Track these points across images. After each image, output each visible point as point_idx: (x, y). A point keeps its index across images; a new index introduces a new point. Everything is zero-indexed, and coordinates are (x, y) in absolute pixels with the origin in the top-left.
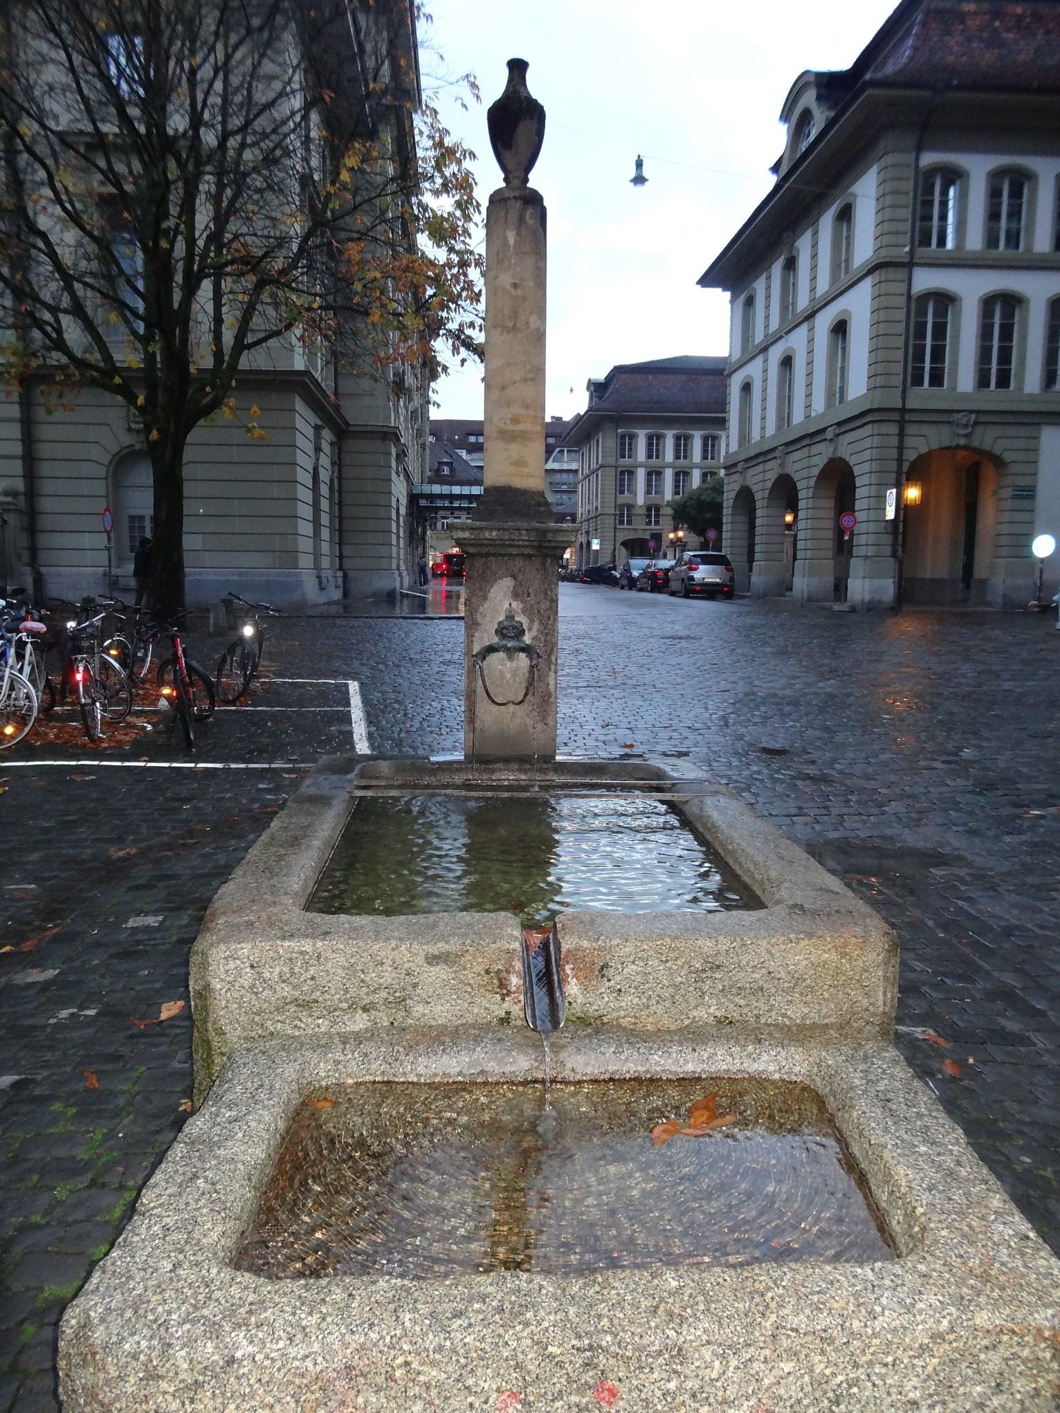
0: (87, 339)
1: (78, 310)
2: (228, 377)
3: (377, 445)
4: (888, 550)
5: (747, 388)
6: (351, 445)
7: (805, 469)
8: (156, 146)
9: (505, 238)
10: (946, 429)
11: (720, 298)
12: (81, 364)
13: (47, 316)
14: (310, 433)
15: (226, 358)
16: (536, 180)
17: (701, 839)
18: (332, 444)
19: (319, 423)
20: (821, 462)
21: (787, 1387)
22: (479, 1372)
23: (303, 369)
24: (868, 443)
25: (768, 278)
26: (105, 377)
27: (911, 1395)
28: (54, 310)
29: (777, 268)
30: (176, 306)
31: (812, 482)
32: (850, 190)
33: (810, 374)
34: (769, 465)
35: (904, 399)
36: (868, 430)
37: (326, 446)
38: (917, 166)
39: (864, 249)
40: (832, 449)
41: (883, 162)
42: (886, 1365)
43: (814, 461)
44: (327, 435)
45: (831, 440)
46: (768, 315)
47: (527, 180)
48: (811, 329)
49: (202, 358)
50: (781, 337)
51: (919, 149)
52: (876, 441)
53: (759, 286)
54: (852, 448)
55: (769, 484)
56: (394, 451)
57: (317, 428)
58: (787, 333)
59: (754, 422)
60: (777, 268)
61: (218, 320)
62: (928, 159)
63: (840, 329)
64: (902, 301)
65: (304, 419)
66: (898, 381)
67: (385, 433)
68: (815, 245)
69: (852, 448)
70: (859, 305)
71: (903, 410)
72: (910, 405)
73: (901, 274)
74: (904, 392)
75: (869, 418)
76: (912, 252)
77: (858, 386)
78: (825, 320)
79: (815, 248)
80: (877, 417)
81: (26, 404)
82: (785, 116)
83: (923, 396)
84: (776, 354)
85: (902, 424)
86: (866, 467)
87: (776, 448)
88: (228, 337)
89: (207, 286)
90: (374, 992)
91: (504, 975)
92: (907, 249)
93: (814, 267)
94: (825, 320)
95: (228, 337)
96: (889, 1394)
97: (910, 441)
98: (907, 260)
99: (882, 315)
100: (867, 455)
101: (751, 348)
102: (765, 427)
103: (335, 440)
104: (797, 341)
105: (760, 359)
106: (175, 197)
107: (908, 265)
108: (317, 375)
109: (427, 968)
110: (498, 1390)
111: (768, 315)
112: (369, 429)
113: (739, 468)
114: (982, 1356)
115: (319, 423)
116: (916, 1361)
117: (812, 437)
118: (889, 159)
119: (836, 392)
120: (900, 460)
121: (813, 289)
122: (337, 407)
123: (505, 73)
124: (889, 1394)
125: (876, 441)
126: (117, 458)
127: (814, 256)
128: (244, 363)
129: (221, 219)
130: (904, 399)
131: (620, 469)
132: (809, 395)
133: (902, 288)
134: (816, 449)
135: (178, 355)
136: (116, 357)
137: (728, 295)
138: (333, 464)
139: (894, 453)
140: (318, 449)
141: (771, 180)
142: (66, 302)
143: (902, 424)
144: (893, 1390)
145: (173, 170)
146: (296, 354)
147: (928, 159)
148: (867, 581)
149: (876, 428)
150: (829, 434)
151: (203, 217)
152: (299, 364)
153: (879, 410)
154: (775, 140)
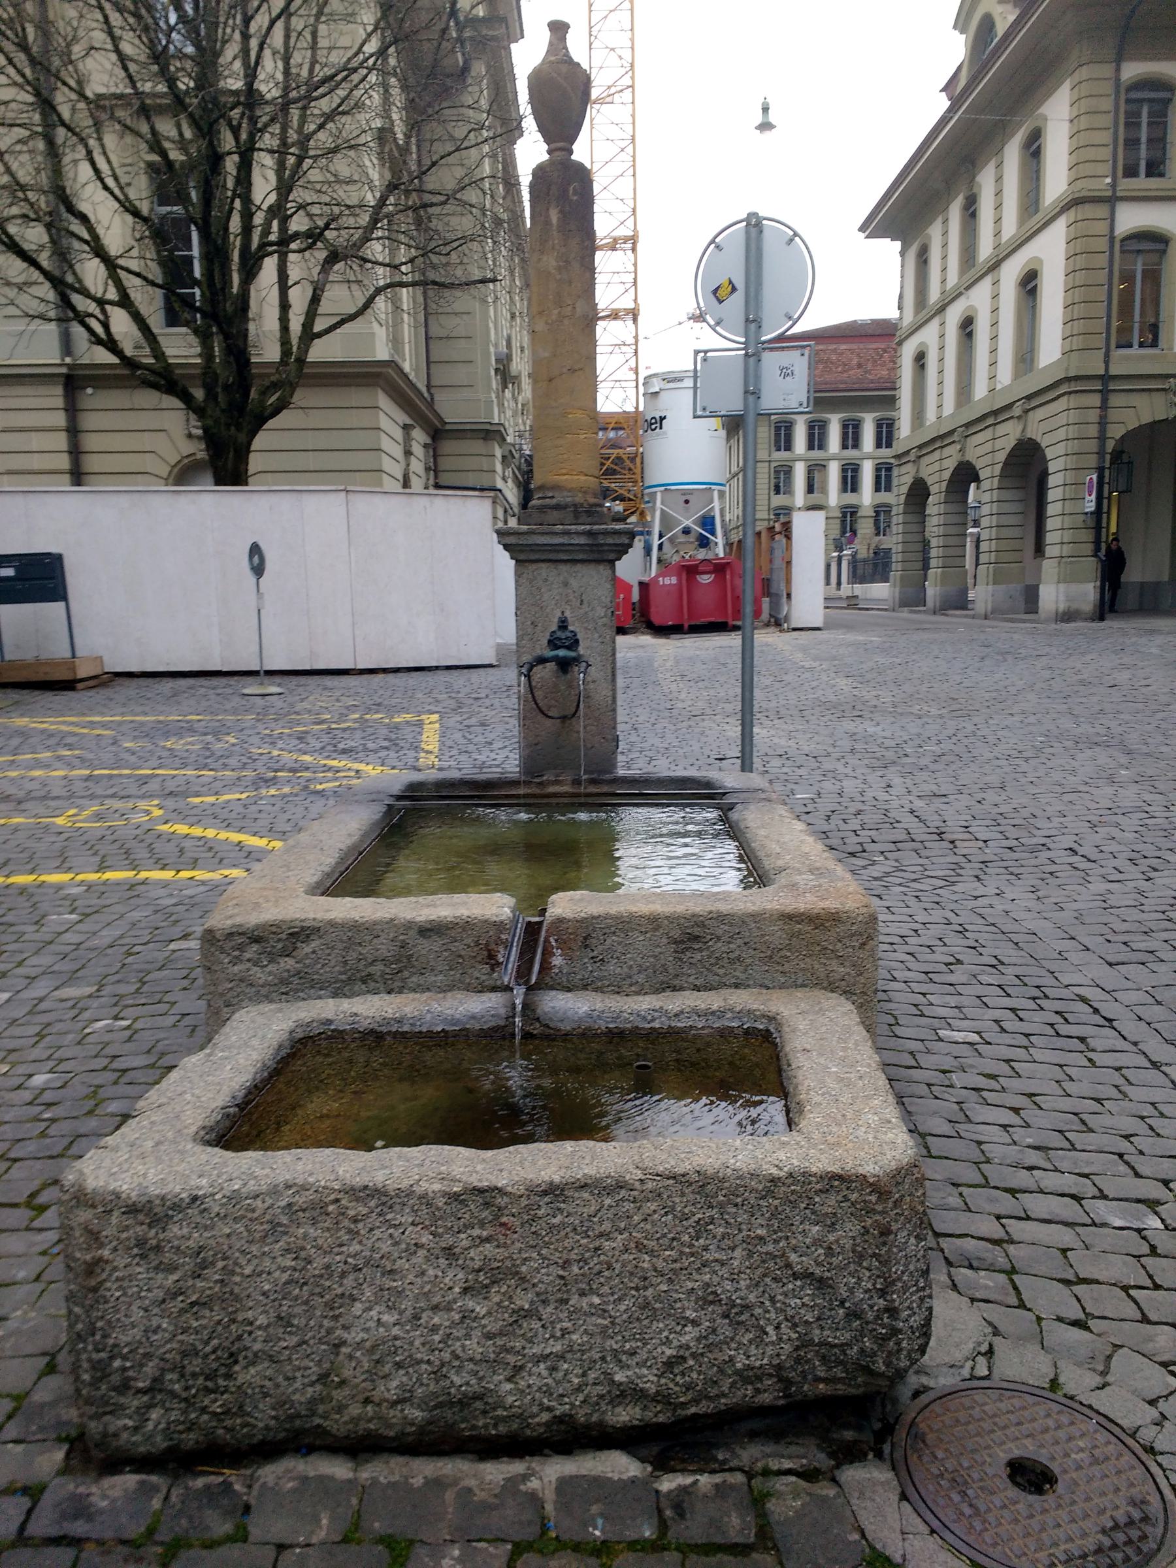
0: (136, 333)
1: (125, 302)
2: (296, 373)
3: (477, 446)
4: (1089, 548)
5: (920, 359)
6: (448, 446)
7: (990, 451)
8: (208, 114)
9: (548, 216)
10: (1159, 399)
11: (890, 248)
12: (127, 361)
13: (92, 307)
14: (398, 434)
15: (295, 349)
16: (580, 152)
17: (741, 846)
18: (425, 446)
19: (409, 421)
20: (1009, 443)
21: (654, 1224)
22: (397, 1208)
23: (386, 358)
24: (1062, 419)
25: (946, 221)
26: (165, 379)
27: (759, 1232)
28: (101, 302)
29: (955, 211)
30: (235, 290)
31: (998, 469)
32: (1040, 111)
33: (994, 338)
34: (947, 451)
35: (1107, 363)
36: (1062, 403)
37: (418, 450)
38: (1118, 79)
39: (1056, 182)
40: (1021, 427)
41: (1077, 77)
42: (736, 1205)
43: (999, 444)
44: (419, 436)
45: (1019, 417)
46: (946, 267)
47: (571, 152)
48: (996, 283)
49: (266, 349)
50: (960, 294)
51: (1119, 60)
52: (1073, 416)
53: (935, 231)
54: (1045, 427)
55: (947, 475)
56: (498, 453)
57: (406, 428)
58: (968, 288)
59: (931, 402)
60: (955, 211)
61: (285, 306)
62: (1132, 70)
63: (1029, 283)
64: (1103, 244)
65: (389, 418)
66: (1100, 341)
67: (488, 431)
68: (999, 179)
69: (1045, 427)
70: (1051, 250)
71: (1106, 378)
72: (1113, 371)
73: (1101, 211)
74: (1107, 355)
75: (1064, 388)
76: (1114, 185)
77: (1051, 348)
78: (1012, 271)
79: (999, 185)
80: (1074, 387)
81: (72, 410)
82: (961, 24)
83: (1129, 361)
84: (954, 315)
85: (1105, 394)
86: (1060, 449)
87: (954, 431)
88: (296, 326)
89: (270, 265)
90: (371, 964)
91: (493, 946)
92: (1109, 180)
93: (998, 207)
94: (1012, 271)
95: (296, 326)
96: (740, 1230)
97: (1113, 415)
98: (1109, 193)
99: (1080, 261)
100: (1061, 434)
101: (924, 305)
102: (942, 406)
103: (429, 441)
104: (979, 298)
105: (935, 322)
106: (231, 164)
107: (1111, 200)
108: (407, 367)
109: (421, 940)
110: (413, 1224)
111: (946, 267)
112: (468, 427)
113: (912, 456)
114: (817, 1199)
115: (409, 421)
116: (761, 1202)
117: (996, 415)
118: (1084, 73)
119: (1026, 356)
120: (1102, 438)
121: (997, 234)
122: (431, 404)
123: (546, 35)
124: (740, 1230)
125: (1073, 416)
126: (176, 470)
127: (999, 193)
128: (318, 352)
129: (285, 188)
130: (1107, 363)
131: (773, 465)
132: (993, 364)
133: (1102, 228)
134: (1001, 429)
135: (238, 352)
136: (169, 352)
137: (898, 245)
138: (427, 469)
139: (1093, 431)
140: (408, 453)
141: (944, 103)
142: (112, 294)
143: (1105, 394)
144: (744, 1227)
145: (227, 141)
146: (379, 338)
147: (1132, 70)
148: (1062, 586)
149: (1074, 401)
150: (1017, 411)
151: (263, 189)
152: (382, 353)
153: (1077, 378)
154: (952, 51)
